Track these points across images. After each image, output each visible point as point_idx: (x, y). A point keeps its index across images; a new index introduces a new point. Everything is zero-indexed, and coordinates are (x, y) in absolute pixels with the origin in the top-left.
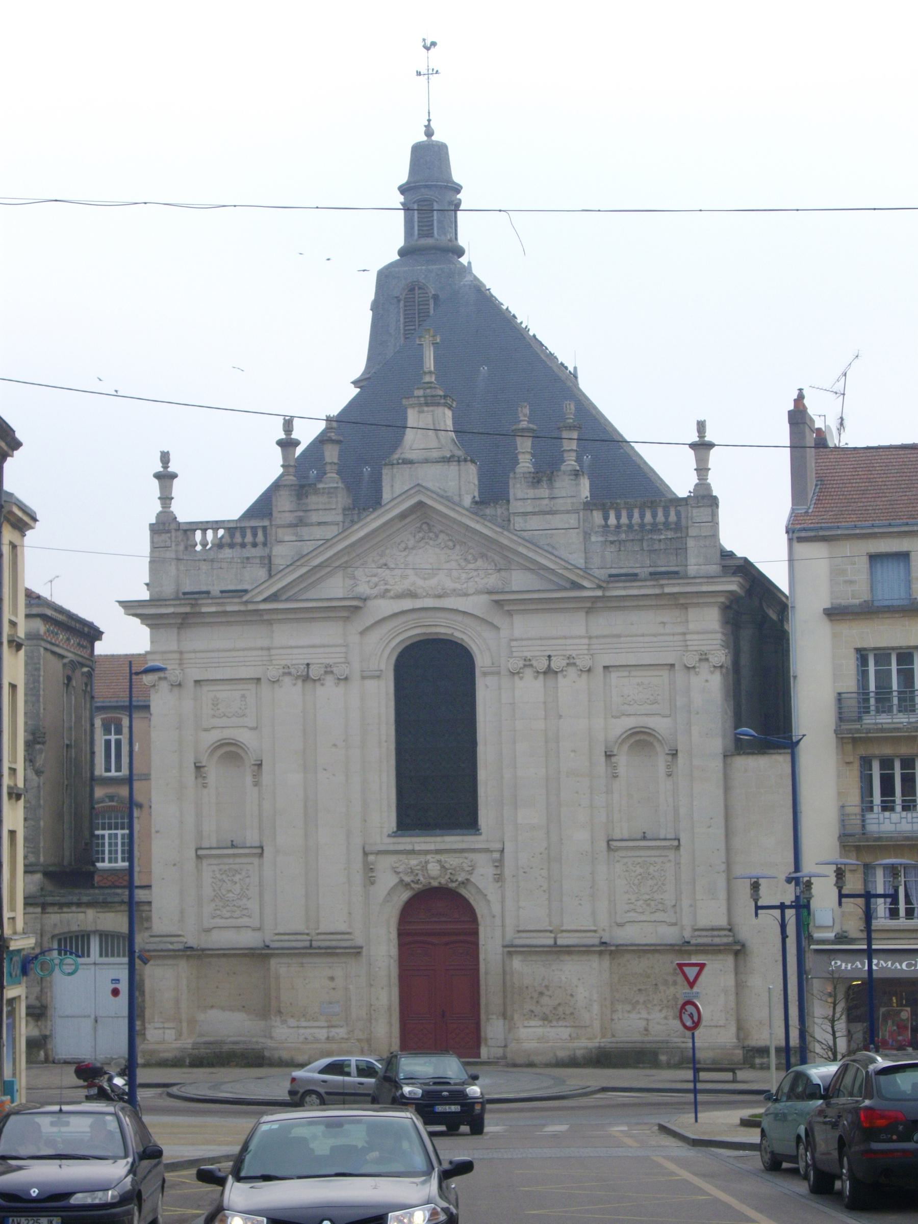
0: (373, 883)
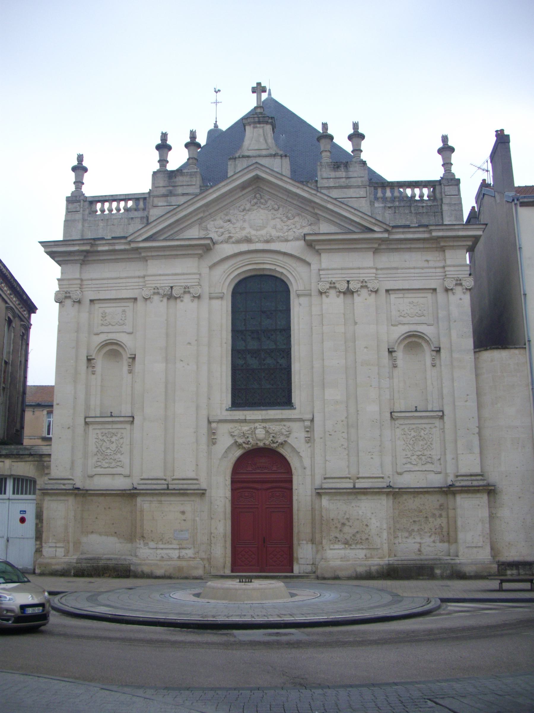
0: (214, 444)
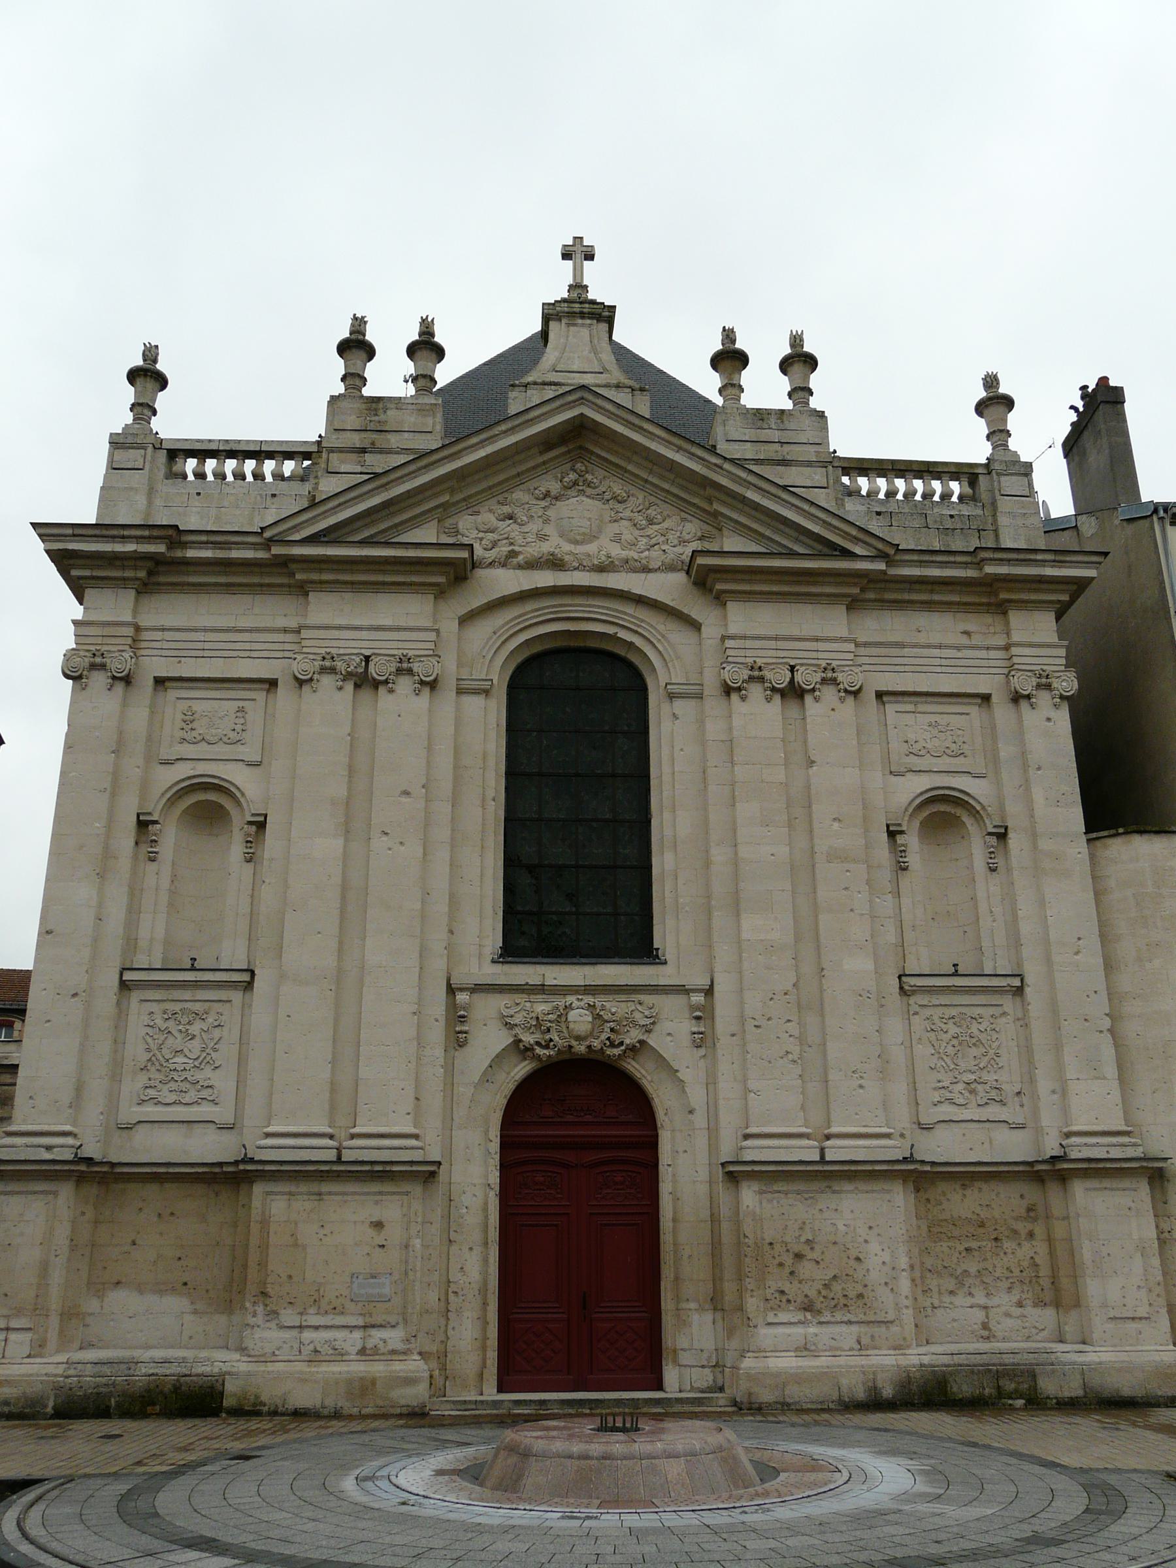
0: (461, 1044)
